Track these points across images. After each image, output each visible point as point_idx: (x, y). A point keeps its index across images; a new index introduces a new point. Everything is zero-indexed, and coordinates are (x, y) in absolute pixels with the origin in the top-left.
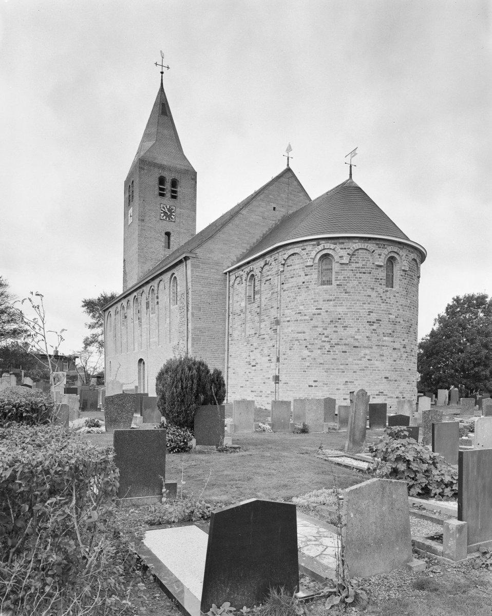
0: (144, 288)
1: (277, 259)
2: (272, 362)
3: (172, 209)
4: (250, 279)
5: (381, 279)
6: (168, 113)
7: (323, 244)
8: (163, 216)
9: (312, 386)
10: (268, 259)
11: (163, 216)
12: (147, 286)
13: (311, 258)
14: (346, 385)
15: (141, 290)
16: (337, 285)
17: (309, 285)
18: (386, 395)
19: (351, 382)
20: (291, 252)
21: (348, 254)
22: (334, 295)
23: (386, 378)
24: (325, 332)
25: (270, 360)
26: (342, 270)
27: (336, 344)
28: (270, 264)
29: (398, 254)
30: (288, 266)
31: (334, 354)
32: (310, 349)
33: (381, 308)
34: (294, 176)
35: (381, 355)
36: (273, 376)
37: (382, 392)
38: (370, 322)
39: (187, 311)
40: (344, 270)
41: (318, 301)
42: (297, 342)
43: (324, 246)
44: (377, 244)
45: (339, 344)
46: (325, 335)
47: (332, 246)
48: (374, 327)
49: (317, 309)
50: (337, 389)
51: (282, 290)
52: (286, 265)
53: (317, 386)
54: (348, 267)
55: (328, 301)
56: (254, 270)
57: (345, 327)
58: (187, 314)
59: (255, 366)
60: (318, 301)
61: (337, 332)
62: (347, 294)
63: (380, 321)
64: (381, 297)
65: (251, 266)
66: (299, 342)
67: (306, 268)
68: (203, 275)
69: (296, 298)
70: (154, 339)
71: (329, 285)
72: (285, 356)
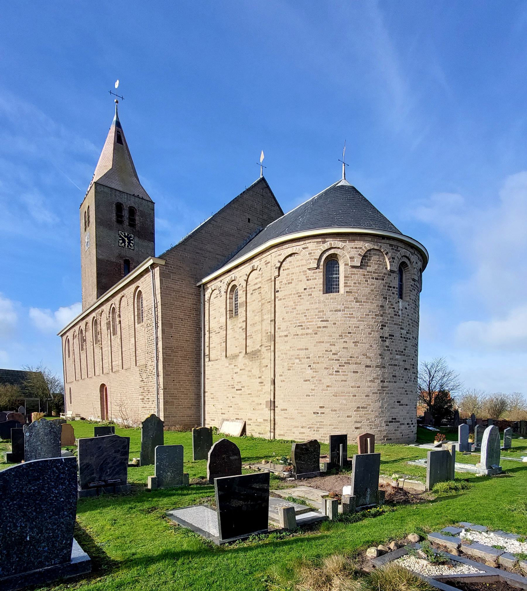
0: (103, 307)
1: (269, 262)
2: (264, 385)
3: (131, 237)
4: (231, 291)
5: (394, 288)
6: (124, 143)
7: (331, 242)
8: (122, 243)
9: (318, 413)
10: (255, 262)
11: (122, 243)
12: (107, 304)
13: (315, 259)
14: (357, 411)
15: (100, 310)
16: (347, 292)
17: (312, 291)
18: (399, 422)
19: (363, 408)
20: (289, 251)
21: (359, 255)
23: (399, 402)
25: (262, 383)
26: (352, 274)
27: (345, 363)
28: (258, 269)
29: (409, 260)
30: (284, 270)
31: (343, 375)
32: (314, 369)
33: (394, 321)
34: (268, 187)
35: (393, 376)
36: (267, 402)
37: (395, 419)
38: (383, 337)
40: (354, 274)
42: (297, 361)
43: (331, 244)
44: (391, 245)
46: (333, 352)
48: (387, 343)
49: (322, 321)
50: (348, 417)
53: (323, 413)
54: (359, 271)
55: (336, 311)
56: (237, 280)
57: (356, 342)
59: (241, 390)
61: (347, 348)
62: (358, 304)
63: (393, 336)
64: (394, 308)
65: (232, 275)
67: (309, 271)
68: (173, 286)
69: (295, 308)
70: (117, 362)
71: (336, 292)
72: (282, 378)
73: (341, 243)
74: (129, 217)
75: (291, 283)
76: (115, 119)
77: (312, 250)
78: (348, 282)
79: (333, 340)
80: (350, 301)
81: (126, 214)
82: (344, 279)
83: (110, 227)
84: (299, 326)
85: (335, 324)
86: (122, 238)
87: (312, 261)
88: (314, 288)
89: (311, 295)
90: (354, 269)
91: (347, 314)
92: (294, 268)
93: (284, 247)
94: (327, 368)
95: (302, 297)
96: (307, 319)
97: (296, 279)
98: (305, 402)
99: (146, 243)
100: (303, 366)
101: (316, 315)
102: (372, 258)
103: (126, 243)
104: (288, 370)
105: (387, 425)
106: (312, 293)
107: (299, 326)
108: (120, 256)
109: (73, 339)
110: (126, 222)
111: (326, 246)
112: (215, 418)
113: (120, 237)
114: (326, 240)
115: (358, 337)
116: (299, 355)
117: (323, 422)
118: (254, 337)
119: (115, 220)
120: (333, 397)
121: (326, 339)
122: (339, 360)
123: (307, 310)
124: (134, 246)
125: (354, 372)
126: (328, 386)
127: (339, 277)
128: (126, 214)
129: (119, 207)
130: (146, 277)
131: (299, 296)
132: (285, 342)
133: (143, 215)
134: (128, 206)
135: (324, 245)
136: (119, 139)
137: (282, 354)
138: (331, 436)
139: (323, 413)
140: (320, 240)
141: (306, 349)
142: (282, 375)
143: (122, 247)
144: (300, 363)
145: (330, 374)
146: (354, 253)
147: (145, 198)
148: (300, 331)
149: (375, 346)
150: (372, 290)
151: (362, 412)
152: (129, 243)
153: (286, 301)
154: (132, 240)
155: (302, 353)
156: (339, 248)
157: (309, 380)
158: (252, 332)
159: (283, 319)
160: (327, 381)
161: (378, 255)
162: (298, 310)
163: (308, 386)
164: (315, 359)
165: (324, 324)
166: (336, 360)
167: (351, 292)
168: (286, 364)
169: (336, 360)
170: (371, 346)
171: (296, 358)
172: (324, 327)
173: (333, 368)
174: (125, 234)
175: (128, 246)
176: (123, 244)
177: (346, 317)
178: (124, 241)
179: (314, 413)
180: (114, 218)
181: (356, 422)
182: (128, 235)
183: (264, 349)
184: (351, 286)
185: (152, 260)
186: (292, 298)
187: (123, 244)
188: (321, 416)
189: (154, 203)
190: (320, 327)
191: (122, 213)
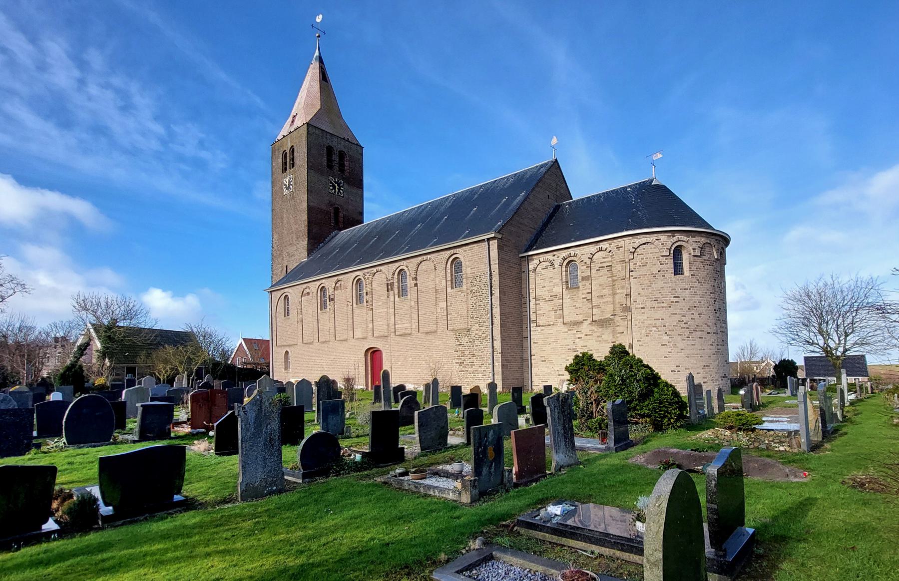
3: (341, 183)
7: (678, 236)
8: (332, 190)
9: (675, 371)
13: (667, 249)
16: (692, 275)
17: (665, 273)
19: (707, 366)
22: (690, 285)
24: (684, 318)
27: (694, 330)
31: (693, 340)
32: (670, 335)
39: (492, 294)
41: (675, 289)
42: (655, 328)
44: (716, 240)
45: (696, 331)
46: (685, 322)
47: (685, 239)
48: (718, 315)
50: (698, 373)
51: (631, 278)
52: (635, 254)
53: (679, 371)
55: (684, 289)
58: (491, 299)
60: (675, 289)
61: (694, 319)
66: (657, 329)
72: (640, 343)
73: (686, 238)
74: (339, 162)
75: (646, 265)
76: (317, 54)
77: (664, 242)
78: (692, 267)
79: (684, 312)
80: (694, 282)
81: (336, 158)
82: (689, 265)
83: (321, 173)
84: (655, 300)
85: (684, 299)
86: (333, 184)
87: (665, 250)
88: (667, 271)
89: (664, 276)
90: (695, 258)
91: (692, 292)
92: (648, 254)
93: (638, 237)
94: (681, 335)
95: (657, 277)
96: (662, 295)
97: (650, 263)
98: (663, 362)
99: (354, 190)
100: (659, 333)
101: (669, 292)
102: (706, 250)
103: (337, 190)
104: (646, 336)
105: (722, 380)
106: (666, 275)
107: (655, 300)
108: (331, 204)
109: (302, 296)
110: (337, 167)
111: (675, 239)
112: (549, 379)
113: (331, 183)
114: (675, 235)
115: (701, 310)
116: (656, 324)
117: (679, 378)
118: (603, 307)
119: (326, 164)
120: (686, 358)
121: (678, 311)
122: (689, 328)
123: (661, 288)
124: (343, 193)
125: (700, 338)
126: (682, 349)
127: (682, 263)
128: (336, 158)
129: (330, 150)
130: (475, 247)
131: (653, 277)
132: (643, 313)
133: (352, 160)
134: (339, 150)
135: (674, 238)
136: (324, 77)
137: (639, 323)
138: (373, 412)
139: (679, 371)
140: (670, 234)
141: (662, 319)
142: (640, 341)
143: (332, 193)
144: (657, 330)
145: (683, 340)
146: (695, 245)
147: (354, 142)
148: (656, 305)
149: (711, 317)
150: (707, 274)
151: (707, 370)
152: (339, 189)
153: (641, 280)
154: (342, 186)
155: (659, 323)
156: (684, 241)
157: (666, 345)
158: (600, 303)
159: (639, 294)
160: (681, 345)
161: (709, 247)
162: (653, 288)
163: (666, 350)
164: (670, 327)
165: (677, 299)
166: (687, 328)
167: (694, 275)
168: (643, 331)
169: (687, 328)
170: (709, 317)
171: (654, 327)
172: (676, 302)
173: (685, 335)
174: (335, 179)
175: (338, 193)
176: (333, 191)
177: (692, 294)
178: (334, 188)
179: (672, 371)
180: (325, 163)
181: (704, 378)
182: (338, 181)
183: (617, 318)
184: (694, 271)
185: (494, 234)
186: (647, 277)
187: (333, 191)
188: (678, 374)
189: (363, 148)
190: (673, 302)
191: (332, 157)
